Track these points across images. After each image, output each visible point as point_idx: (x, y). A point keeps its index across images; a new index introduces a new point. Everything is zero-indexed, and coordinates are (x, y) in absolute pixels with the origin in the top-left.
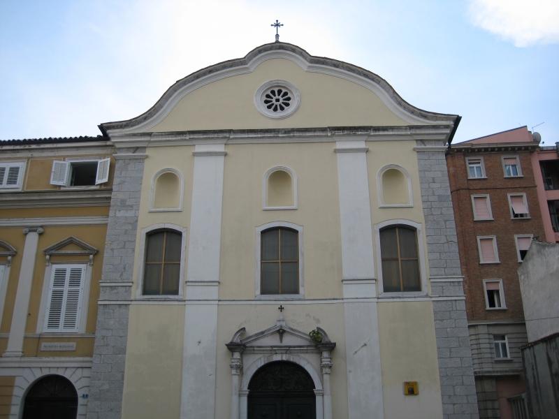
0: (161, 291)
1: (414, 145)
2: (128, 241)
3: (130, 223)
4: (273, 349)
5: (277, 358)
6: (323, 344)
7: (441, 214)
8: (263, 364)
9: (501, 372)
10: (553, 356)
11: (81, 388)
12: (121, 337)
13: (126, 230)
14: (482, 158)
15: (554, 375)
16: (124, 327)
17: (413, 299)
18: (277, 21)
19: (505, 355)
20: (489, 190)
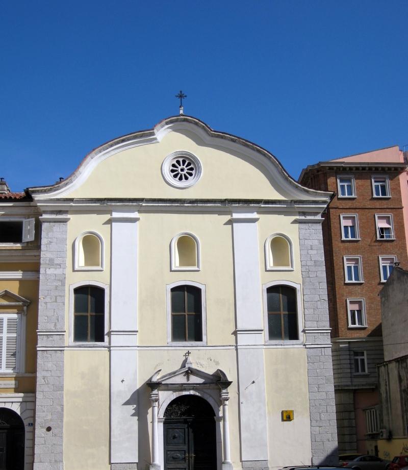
0: (293, 313)
2: (60, 296)
3: (59, 280)
4: (182, 387)
6: (222, 383)
7: (316, 277)
8: (175, 398)
9: (358, 385)
10: (403, 373)
11: (26, 418)
12: (59, 377)
13: (57, 287)
14: (352, 176)
15: (403, 391)
16: (60, 369)
17: (292, 346)
18: (181, 92)
19: (363, 370)
20: (357, 210)
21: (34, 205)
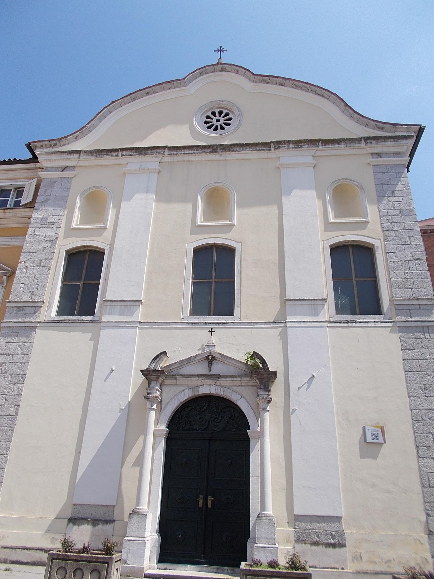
0: (374, 279)
1: (370, 159)
5: (204, 391)
18: (221, 47)
21: (41, 166)
